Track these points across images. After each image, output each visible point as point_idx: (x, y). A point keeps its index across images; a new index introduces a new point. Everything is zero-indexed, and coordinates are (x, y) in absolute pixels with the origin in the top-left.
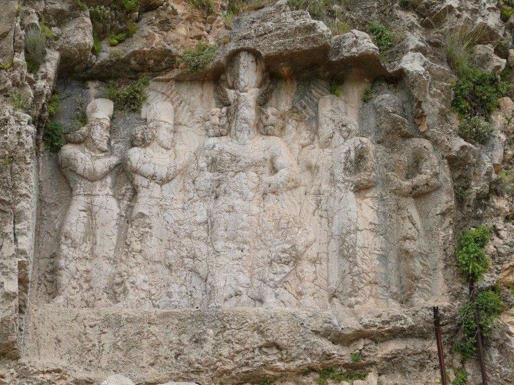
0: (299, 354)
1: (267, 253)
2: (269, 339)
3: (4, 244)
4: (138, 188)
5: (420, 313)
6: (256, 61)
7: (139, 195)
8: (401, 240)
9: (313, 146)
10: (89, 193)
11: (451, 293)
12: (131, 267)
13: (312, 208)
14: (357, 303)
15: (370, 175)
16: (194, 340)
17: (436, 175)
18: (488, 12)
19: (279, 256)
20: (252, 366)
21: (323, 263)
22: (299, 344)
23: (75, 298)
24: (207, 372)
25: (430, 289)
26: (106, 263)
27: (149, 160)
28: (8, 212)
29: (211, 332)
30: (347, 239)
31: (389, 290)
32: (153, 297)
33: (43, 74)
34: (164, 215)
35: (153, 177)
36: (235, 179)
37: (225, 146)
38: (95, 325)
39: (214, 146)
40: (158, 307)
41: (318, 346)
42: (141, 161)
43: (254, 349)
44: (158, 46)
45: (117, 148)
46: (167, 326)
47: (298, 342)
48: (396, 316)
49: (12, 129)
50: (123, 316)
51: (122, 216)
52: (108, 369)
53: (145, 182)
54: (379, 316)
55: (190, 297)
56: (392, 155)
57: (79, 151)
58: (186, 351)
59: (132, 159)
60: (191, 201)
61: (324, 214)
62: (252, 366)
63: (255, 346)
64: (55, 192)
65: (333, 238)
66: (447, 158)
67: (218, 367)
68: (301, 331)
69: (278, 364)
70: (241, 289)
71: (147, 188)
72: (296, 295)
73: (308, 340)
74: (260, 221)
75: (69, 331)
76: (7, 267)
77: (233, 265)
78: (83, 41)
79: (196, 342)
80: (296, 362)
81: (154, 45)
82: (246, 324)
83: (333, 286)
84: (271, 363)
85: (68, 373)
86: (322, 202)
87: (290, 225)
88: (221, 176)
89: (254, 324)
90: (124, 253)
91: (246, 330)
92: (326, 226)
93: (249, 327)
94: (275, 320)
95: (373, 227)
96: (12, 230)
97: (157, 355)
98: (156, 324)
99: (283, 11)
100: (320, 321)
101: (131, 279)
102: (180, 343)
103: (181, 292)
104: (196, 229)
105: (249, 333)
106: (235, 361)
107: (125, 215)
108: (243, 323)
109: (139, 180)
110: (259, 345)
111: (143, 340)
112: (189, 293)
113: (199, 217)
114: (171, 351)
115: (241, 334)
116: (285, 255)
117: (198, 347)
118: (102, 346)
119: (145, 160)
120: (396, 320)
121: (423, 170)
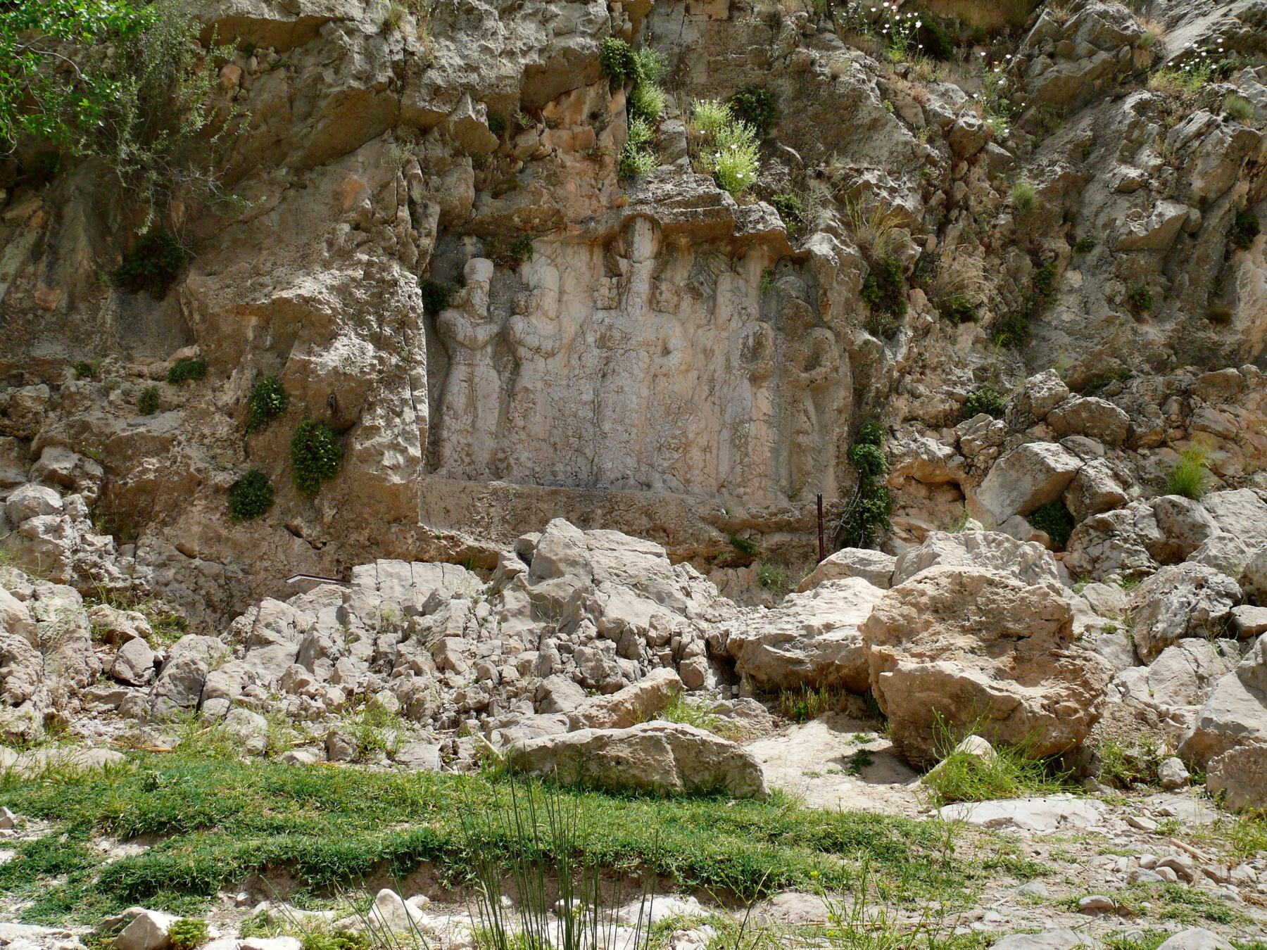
54: (767, 508)
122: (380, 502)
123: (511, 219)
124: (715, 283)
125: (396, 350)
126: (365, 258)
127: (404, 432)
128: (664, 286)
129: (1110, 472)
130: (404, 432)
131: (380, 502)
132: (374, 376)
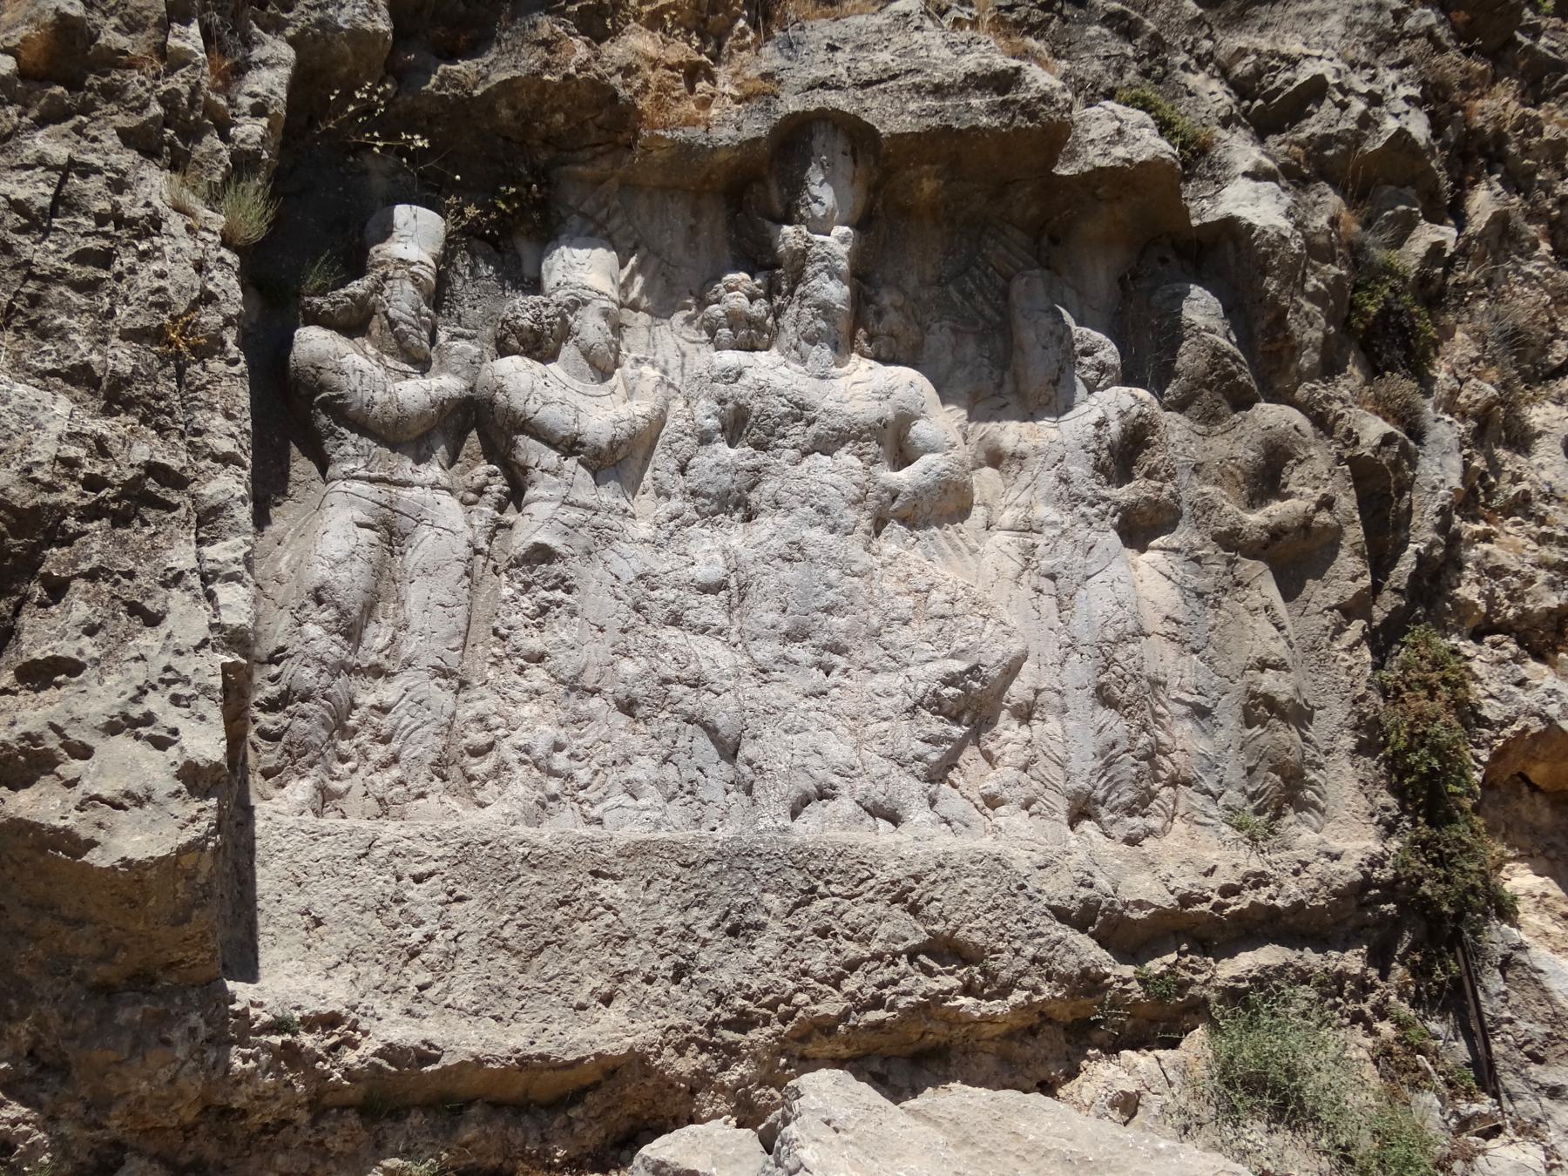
0: (1022, 974)
1: (901, 680)
2: (936, 927)
3: (171, 603)
5: (1315, 868)
6: (854, 153)
7: (530, 493)
8: (1251, 668)
9: (1002, 401)
11: (1376, 819)
12: (515, 703)
13: (1012, 566)
14: (1150, 832)
15: (1160, 489)
16: (728, 925)
17: (1327, 503)
18: (1406, 108)
19: (935, 693)
20: (892, 1007)
21: (1049, 718)
22: (1017, 944)
23: (348, 790)
24: (767, 1023)
25: (1322, 804)
26: (439, 685)
27: (560, 394)
28: (177, 507)
29: (773, 901)
30: (1120, 656)
31: (1220, 802)
32: (582, 794)
34: (607, 558)
35: (570, 446)
36: (800, 470)
37: (771, 376)
38: (431, 874)
39: (740, 374)
40: (599, 821)
41: (1070, 951)
43: (897, 955)
44: (583, 75)
45: (459, 354)
46: (649, 883)
47: (1015, 938)
48: (1256, 875)
49: (179, 250)
50: (513, 849)
51: (478, 552)
52: (476, 1013)
53: (551, 457)
54: (1211, 872)
55: (689, 798)
56: (1209, 442)
58: (704, 958)
59: (510, 386)
60: (678, 521)
61: (1046, 584)
62: (892, 1007)
63: (900, 947)
65: (1075, 649)
66: (1350, 461)
67: (798, 1008)
68: (1020, 907)
69: (962, 1000)
70: (836, 780)
72: (981, 803)
73: (1041, 935)
74: (876, 592)
75: (348, 891)
76: (186, 681)
77: (808, 710)
79: (733, 932)
80: (1011, 998)
81: (572, 70)
82: (872, 882)
83: (1079, 783)
84: (945, 1000)
85: (363, 1025)
86: (1039, 551)
87: (959, 606)
88: (762, 457)
89: (893, 883)
90: (492, 660)
91: (871, 901)
92: (1054, 617)
93: (878, 892)
94: (947, 872)
95: (1171, 627)
96: (195, 564)
97: (623, 969)
98: (614, 877)
99: (917, 28)
100: (1066, 878)
101: (520, 738)
102: (687, 933)
103: (665, 783)
104: (696, 604)
105: (880, 908)
106: (846, 989)
107: (487, 548)
108: (862, 881)
109: (530, 450)
110: (909, 943)
111: (577, 924)
112: (687, 787)
113: (704, 569)
114: (662, 957)
115: (858, 910)
116: (951, 691)
117: (737, 946)
118: (455, 940)
120: (1256, 886)
121: (1291, 487)
122: (79, 922)
123: (491, 111)
124: (1005, 294)
125: (154, 417)
126: (60, 152)
127: (170, 677)
128: (887, 298)
129: (1184, 710)
130: (170, 677)
131: (79, 922)
132: (70, 494)
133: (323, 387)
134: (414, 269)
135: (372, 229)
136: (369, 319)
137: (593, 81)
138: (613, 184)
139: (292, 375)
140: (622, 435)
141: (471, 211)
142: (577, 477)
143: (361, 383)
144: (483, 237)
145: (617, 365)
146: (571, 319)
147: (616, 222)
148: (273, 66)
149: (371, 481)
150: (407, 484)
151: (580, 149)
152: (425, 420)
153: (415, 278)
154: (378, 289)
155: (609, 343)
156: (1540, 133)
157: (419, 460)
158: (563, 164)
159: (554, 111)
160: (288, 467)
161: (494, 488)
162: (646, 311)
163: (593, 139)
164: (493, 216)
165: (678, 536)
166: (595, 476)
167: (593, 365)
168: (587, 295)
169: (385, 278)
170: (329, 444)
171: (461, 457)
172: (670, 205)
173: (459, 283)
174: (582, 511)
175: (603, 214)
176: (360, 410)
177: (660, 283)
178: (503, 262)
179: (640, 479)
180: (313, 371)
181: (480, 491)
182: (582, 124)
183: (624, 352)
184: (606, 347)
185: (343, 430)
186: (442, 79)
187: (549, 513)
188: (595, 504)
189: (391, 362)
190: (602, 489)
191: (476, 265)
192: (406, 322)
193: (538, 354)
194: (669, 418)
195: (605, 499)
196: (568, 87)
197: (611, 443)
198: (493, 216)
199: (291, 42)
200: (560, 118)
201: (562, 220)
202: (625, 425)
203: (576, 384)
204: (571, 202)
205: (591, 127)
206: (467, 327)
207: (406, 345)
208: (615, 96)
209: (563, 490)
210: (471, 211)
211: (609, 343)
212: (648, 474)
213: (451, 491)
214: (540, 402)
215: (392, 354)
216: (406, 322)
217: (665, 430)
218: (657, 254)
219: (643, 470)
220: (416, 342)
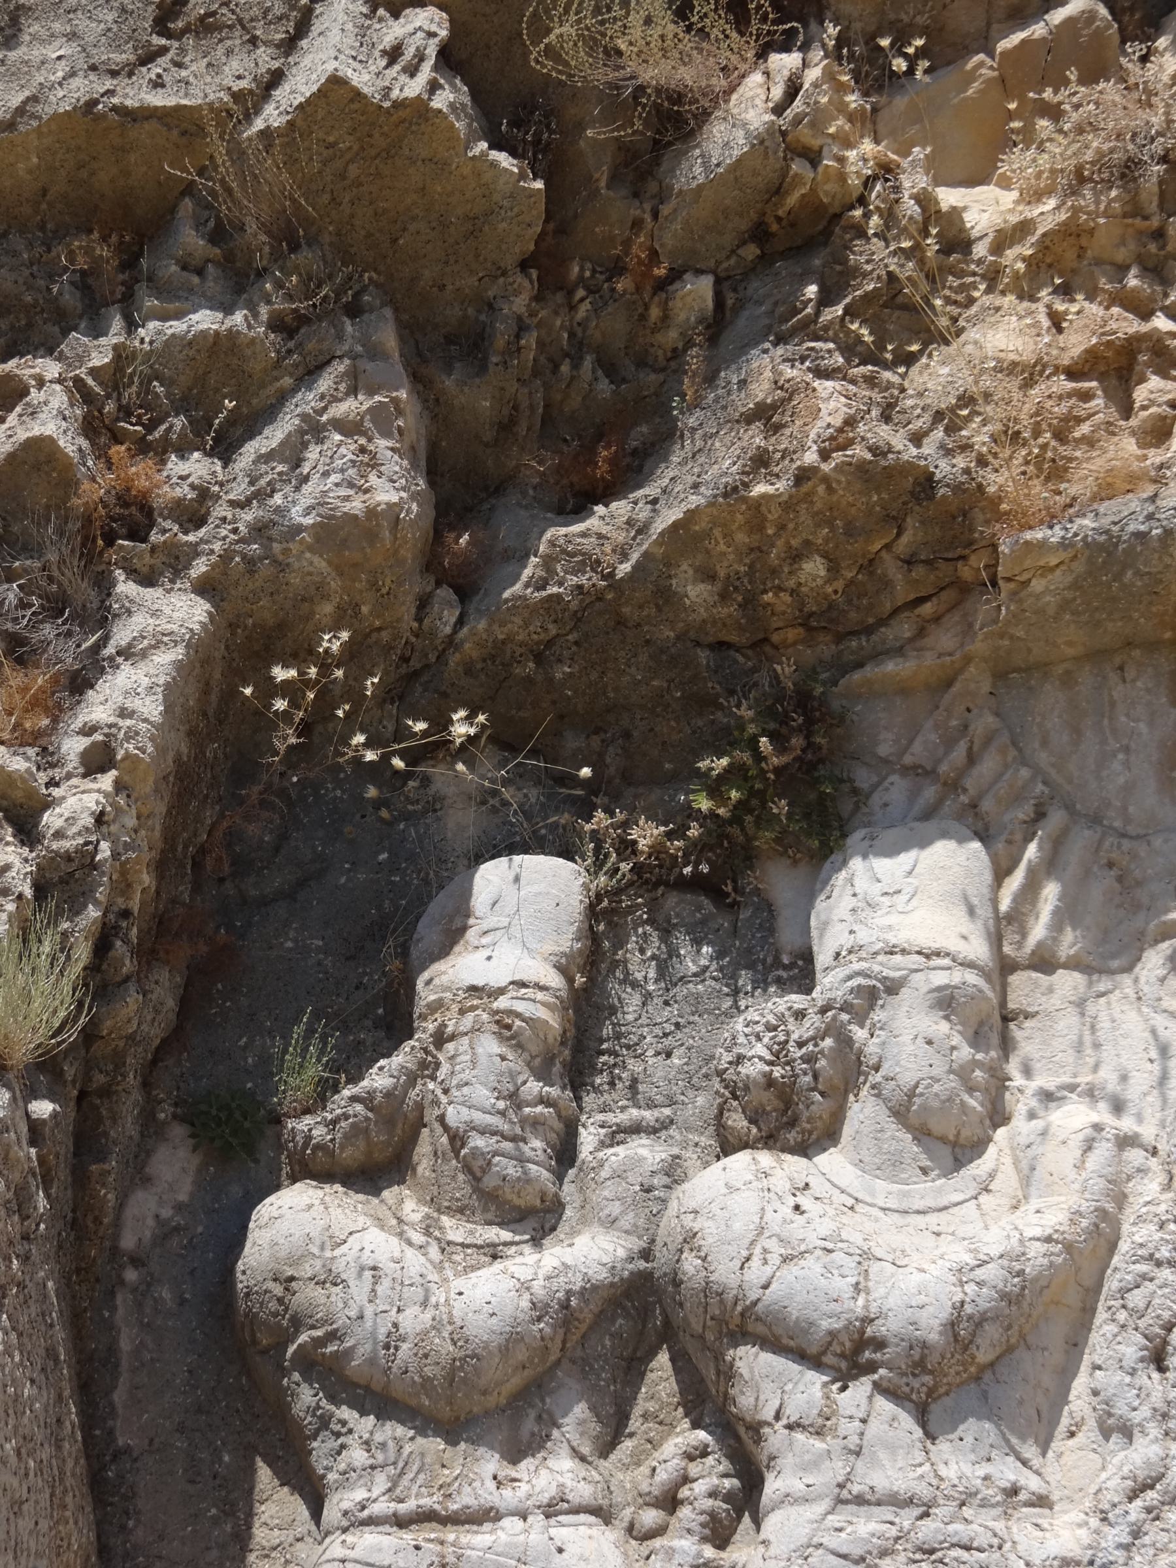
4: (758, 1439)
7: (773, 1486)
10: (426, 1502)
27: (825, 1227)
33: (77, 724)
42: (772, 1244)
45: (618, 1175)
57: (362, 1221)
59: (710, 1231)
60: (1151, 1496)
64: (215, 1521)
71: (819, 1433)
78: (356, 506)
81: (810, 457)
119: (797, 1227)
123: (665, 597)
133: (297, 1323)
134: (502, 1003)
135: (427, 931)
136: (412, 1139)
137: (862, 468)
138: (977, 679)
139: (242, 1306)
140: (980, 1298)
141: (646, 834)
142: (875, 1427)
143: (373, 1296)
144: (684, 885)
145: (998, 1116)
146: (859, 1034)
147: (988, 766)
148: (144, 654)
149: (401, 1522)
150: (485, 1516)
151: (883, 622)
152: (521, 1355)
153: (503, 1026)
154: (427, 1068)
155: (963, 1073)
156: (20, 586)
157: (515, 1454)
158: (846, 669)
159: (796, 557)
160: (250, 1515)
161: (700, 1487)
162: (1074, 964)
163: (902, 593)
164: (694, 832)
165: (1153, 1534)
166: (922, 1416)
167: (922, 1133)
168: (893, 967)
169: (440, 1039)
170: (320, 1448)
171: (634, 1424)
172: (1119, 691)
173: (633, 1001)
174: (887, 1513)
175: (959, 753)
176: (372, 1361)
177: (1101, 886)
178: (735, 931)
179: (1061, 1397)
180: (278, 1290)
181: (670, 1502)
182: (870, 564)
183: (1018, 1080)
184: (952, 1082)
185: (345, 1413)
186: (548, 563)
187: (802, 1534)
188: (923, 1491)
189: (455, 1229)
190: (943, 1447)
191: (673, 953)
192: (483, 1131)
193: (792, 1136)
194: (1126, 1228)
195: (950, 1472)
196: (808, 497)
197: (952, 1325)
198: (694, 832)
199: (204, 588)
200: (814, 568)
201: (860, 797)
202: (986, 1273)
203: (883, 1190)
204: (884, 750)
205: (891, 568)
206: (651, 1105)
207: (489, 1182)
208: (927, 482)
209: (837, 1469)
210: (646, 834)
211: (963, 1073)
212: (1080, 1384)
213: (603, 1513)
214: (774, 1259)
215: (461, 1211)
216: (483, 1131)
217: (1116, 1260)
218: (1095, 820)
219: (1068, 1373)
220: (512, 1170)
